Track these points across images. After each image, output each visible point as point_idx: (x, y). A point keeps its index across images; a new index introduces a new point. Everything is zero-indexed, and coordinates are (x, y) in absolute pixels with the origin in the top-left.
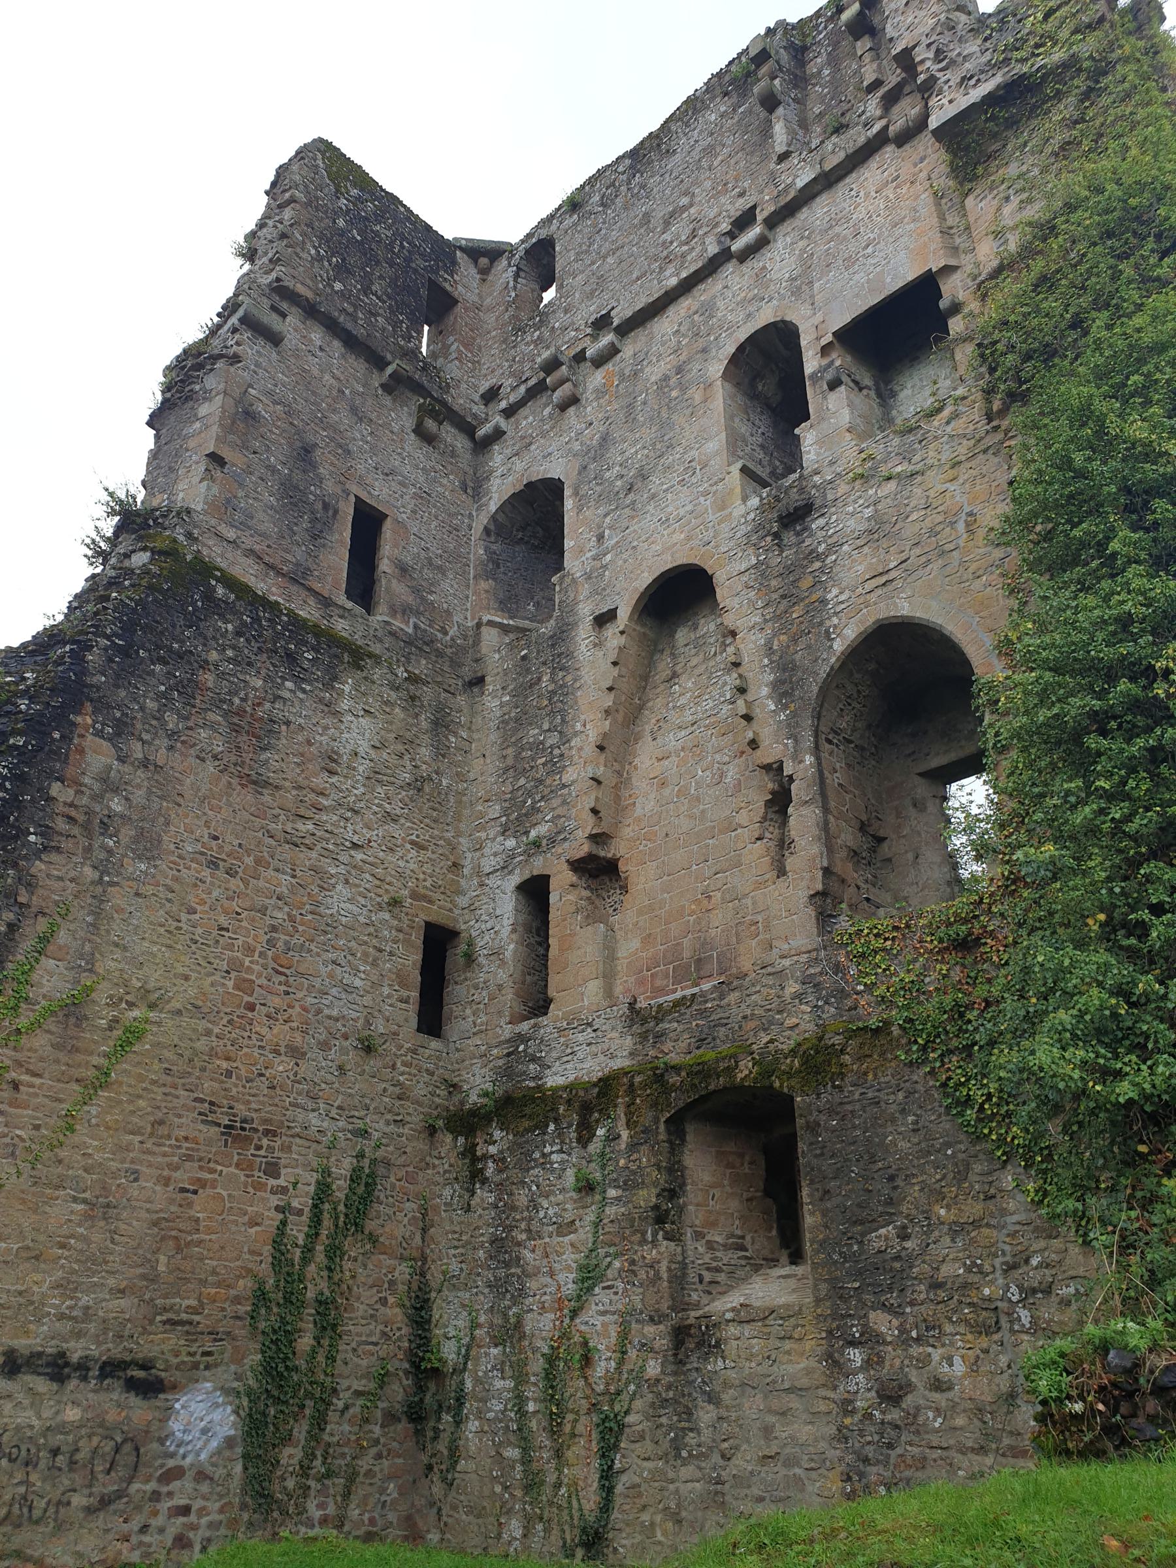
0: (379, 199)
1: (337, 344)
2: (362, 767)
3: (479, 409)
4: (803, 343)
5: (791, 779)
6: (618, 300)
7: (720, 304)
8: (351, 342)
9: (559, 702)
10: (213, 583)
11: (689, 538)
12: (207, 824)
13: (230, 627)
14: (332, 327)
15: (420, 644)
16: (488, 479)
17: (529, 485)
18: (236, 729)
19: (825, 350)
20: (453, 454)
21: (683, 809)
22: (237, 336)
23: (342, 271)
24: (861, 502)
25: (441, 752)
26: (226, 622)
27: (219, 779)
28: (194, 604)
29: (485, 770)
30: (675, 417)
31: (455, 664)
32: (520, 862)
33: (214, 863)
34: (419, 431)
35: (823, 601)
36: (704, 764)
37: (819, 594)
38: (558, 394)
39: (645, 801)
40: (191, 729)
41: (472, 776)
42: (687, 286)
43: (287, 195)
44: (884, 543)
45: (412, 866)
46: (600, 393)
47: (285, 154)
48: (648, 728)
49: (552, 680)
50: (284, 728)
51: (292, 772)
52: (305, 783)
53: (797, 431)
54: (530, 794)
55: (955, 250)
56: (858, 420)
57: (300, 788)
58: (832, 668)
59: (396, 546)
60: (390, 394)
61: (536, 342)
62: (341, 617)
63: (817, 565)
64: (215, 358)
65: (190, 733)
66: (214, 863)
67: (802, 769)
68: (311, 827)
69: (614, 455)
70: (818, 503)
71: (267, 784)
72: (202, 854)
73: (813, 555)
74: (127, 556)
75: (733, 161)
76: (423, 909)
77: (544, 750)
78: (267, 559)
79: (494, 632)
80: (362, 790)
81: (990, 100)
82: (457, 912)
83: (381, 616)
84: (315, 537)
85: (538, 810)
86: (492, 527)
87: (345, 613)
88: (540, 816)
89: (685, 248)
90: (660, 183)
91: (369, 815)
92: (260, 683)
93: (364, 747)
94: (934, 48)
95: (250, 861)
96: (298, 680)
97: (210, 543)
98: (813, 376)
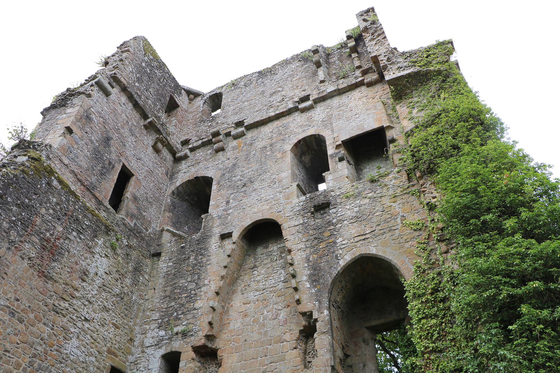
0: (159, 63)
1: (130, 104)
2: (98, 282)
3: (179, 146)
4: (327, 143)
5: (316, 320)
6: (248, 117)
7: (292, 125)
8: (136, 105)
9: (198, 270)
10: (53, 178)
11: (271, 208)
12: (15, 292)
13: (55, 200)
14: (131, 97)
15: (134, 232)
16: (178, 173)
17: (197, 178)
18: (44, 248)
19: (338, 147)
20: (165, 160)
21: (255, 329)
22: (92, 88)
23: (139, 80)
24: (353, 205)
25: (135, 283)
26: (54, 197)
27: (28, 270)
28: (41, 185)
29: (154, 298)
30: (268, 161)
31: (149, 245)
32: (166, 344)
33: (13, 313)
34: (155, 147)
35: (335, 243)
36: (268, 308)
37: (333, 239)
38: (216, 146)
39: (235, 323)
40: (22, 242)
41: (147, 297)
42: (278, 117)
43: (126, 49)
44: (364, 223)
45: (111, 336)
46: (234, 148)
47: (128, 37)
48: (240, 288)
49: (195, 259)
50: (67, 253)
51: (65, 276)
52: (70, 283)
53: (323, 174)
54: (176, 311)
55: (392, 122)
56: (350, 175)
57: (67, 284)
58: (339, 272)
59: (135, 188)
60: (146, 130)
61: (209, 127)
62: (104, 211)
63: (332, 227)
64: (80, 93)
65: (20, 244)
66: (13, 313)
67: (323, 316)
68: (67, 305)
69: (238, 171)
70: (333, 203)
71: (51, 278)
72: (8, 307)
73: (330, 223)
74: (15, 157)
75: (301, 80)
76: (112, 359)
77: (186, 290)
78: (79, 177)
79: (169, 235)
80: (96, 292)
81: (409, 75)
82: (127, 364)
83: (119, 216)
84: (102, 174)
85: (179, 319)
86: (176, 192)
87: (106, 210)
88: (180, 322)
89: (278, 104)
90: (270, 84)
91: (96, 306)
92: (62, 229)
93: (101, 272)
94: (387, 57)
95: (32, 316)
96: (79, 232)
97: (56, 162)
98: (332, 156)
